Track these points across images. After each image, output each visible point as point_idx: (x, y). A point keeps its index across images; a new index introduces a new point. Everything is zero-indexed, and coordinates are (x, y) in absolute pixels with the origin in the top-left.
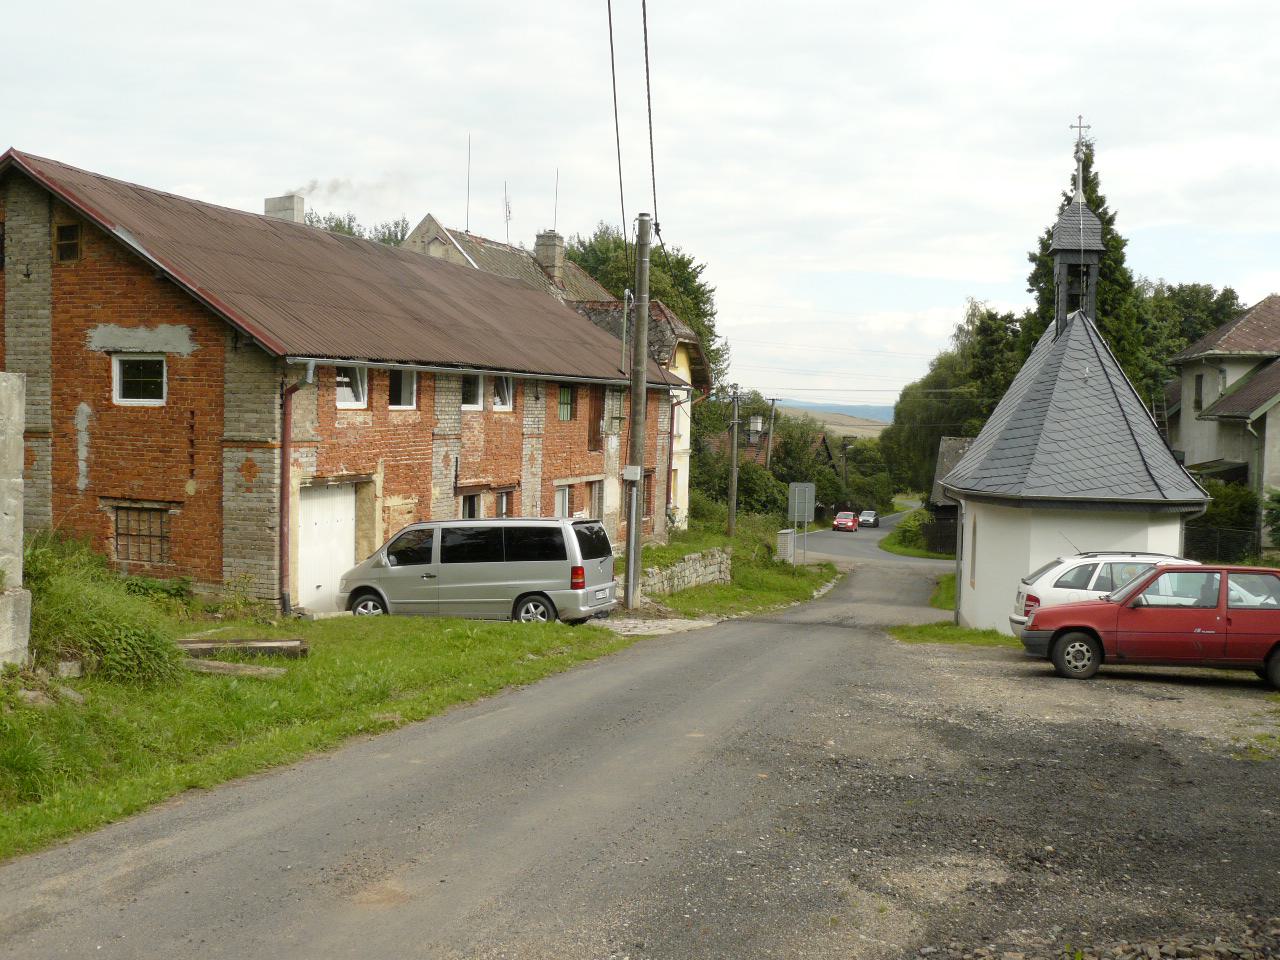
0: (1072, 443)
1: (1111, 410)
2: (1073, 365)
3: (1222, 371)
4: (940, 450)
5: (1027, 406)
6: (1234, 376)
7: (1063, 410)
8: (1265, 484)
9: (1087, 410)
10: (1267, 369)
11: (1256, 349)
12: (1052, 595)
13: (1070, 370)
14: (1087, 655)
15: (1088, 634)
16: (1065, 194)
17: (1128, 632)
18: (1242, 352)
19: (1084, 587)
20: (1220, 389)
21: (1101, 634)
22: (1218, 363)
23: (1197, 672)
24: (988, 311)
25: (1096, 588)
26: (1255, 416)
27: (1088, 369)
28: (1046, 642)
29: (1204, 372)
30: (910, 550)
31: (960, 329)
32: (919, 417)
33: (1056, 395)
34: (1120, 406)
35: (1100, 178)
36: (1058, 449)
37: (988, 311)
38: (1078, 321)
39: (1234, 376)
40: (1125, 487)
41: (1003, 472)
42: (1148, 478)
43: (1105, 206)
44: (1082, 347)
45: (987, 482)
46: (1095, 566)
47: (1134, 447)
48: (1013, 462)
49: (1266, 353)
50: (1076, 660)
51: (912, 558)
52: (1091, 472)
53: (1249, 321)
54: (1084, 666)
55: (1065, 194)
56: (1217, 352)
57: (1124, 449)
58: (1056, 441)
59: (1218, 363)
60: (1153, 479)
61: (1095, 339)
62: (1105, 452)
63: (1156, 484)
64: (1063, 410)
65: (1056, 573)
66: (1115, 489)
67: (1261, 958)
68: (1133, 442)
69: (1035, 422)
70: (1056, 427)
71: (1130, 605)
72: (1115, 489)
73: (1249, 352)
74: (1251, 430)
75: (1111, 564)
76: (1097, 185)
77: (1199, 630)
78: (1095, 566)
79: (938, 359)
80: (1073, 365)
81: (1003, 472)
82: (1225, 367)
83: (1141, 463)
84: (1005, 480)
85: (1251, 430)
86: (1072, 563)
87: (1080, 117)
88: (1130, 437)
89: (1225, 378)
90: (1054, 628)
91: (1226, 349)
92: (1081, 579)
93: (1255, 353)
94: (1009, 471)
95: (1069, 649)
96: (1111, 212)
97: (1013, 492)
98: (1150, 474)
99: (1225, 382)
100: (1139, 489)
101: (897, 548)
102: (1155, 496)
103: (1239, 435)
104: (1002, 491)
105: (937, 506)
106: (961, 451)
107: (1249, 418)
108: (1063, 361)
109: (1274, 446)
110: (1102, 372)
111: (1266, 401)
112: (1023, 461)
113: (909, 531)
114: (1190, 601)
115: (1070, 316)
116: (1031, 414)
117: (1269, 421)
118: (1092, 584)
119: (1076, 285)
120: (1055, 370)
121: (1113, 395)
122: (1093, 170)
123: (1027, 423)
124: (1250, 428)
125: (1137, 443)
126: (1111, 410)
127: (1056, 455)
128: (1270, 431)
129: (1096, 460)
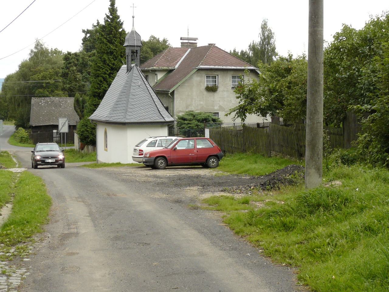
0: (137, 105)
1: (147, 95)
2: (135, 81)
3: (156, 74)
4: (32, 103)
5: (122, 94)
6: (160, 76)
7: (134, 95)
8: (175, 113)
9: (141, 95)
10: (171, 74)
11: (167, 67)
12: (146, 149)
13: (135, 83)
14: (164, 163)
15: (164, 157)
16: (106, 14)
17: (174, 156)
18: (163, 68)
19: (155, 146)
20: (156, 81)
21: (167, 157)
22: (154, 71)
23: (186, 167)
24: (68, 52)
25: (158, 147)
26: (171, 91)
27: (140, 83)
28: (153, 160)
29: (149, 75)
30: (26, 145)
31: (32, 51)
32: (16, 89)
33: (132, 91)
34: (150, 93)
35: (118, 9)
36: (134, 107)
37: (68, 52)
38: (135, 67)
39: (160, 76)
40: (154, 118)
41: (118, 115)
42: (160, 115)
43: (120, 19)
44: (137, 76)
45: (114, 118)
46: (157, 140)
47: (155, 106)
48: (120, 111)
49: (170, 68)
50: (161, 164)
51: (29, 148)
52: (144, 114)
53: (163, 57)
54: (163, 166)
55: (106, 14)
56: (155, 68)
57: (152, 107)
58: (133, 105)
59: (154, 71)
60: (161, 115)
61: (140, 73)
62: (147, 108)
63: (162, 116)
64: (134, 95)
65: (146, 143)
66: (151, 118)
67: (387, 41)
68: (155, 104)
69: (126, 99)
70: (132, 100)
71: (173, 149)
72: (151, 118)
73: (165, 68)
74: (170, 95)
75: (161, 140)
76: (117, 11)
77: (190, 154)
78: (157, 140)
79: (21, 64)
80: (135, 81)
81: (118, 115)
82: (156, 73)
83: (158, 110)
84: (119, 117)
85: (170, 95)
86: (150, 140)
87: (133, 4)
88: (154, 103)
89: (157, 77)
90: (156, 156)
91: (157, 67)
92: (152, 144)
93: (167, 68)
94: (120, 114)
95: (159, 162)
96: (122, 21)
97: (123, 121)
98: (160, 114)
99: (157, 78)
100: (158, 118)
101: (19, 144)
102: (163, 120)
103: (164, 97)
104: (119, 121)
105: (33, 126)
106: (40, 103)
107: (169, 92)
108: (133, 80)
109: (177, 101)
110: (144, 83)
111: (174, 86)
112: (124, 111)
113: (24, 137)
114: (184, 148)
115: (132, 65)
116: (124, 96)
117: (175, 92)
118: (156, 146)
119: (133, 56)
120: (130, 83)
121: (148, 90)
122: (116, 6)
123: (123, 99)
124: (169, 95)
125: (156, 105)
126: (147, 95)
127: (134, 109)
128: (176, 96)
129: (145, 110)
